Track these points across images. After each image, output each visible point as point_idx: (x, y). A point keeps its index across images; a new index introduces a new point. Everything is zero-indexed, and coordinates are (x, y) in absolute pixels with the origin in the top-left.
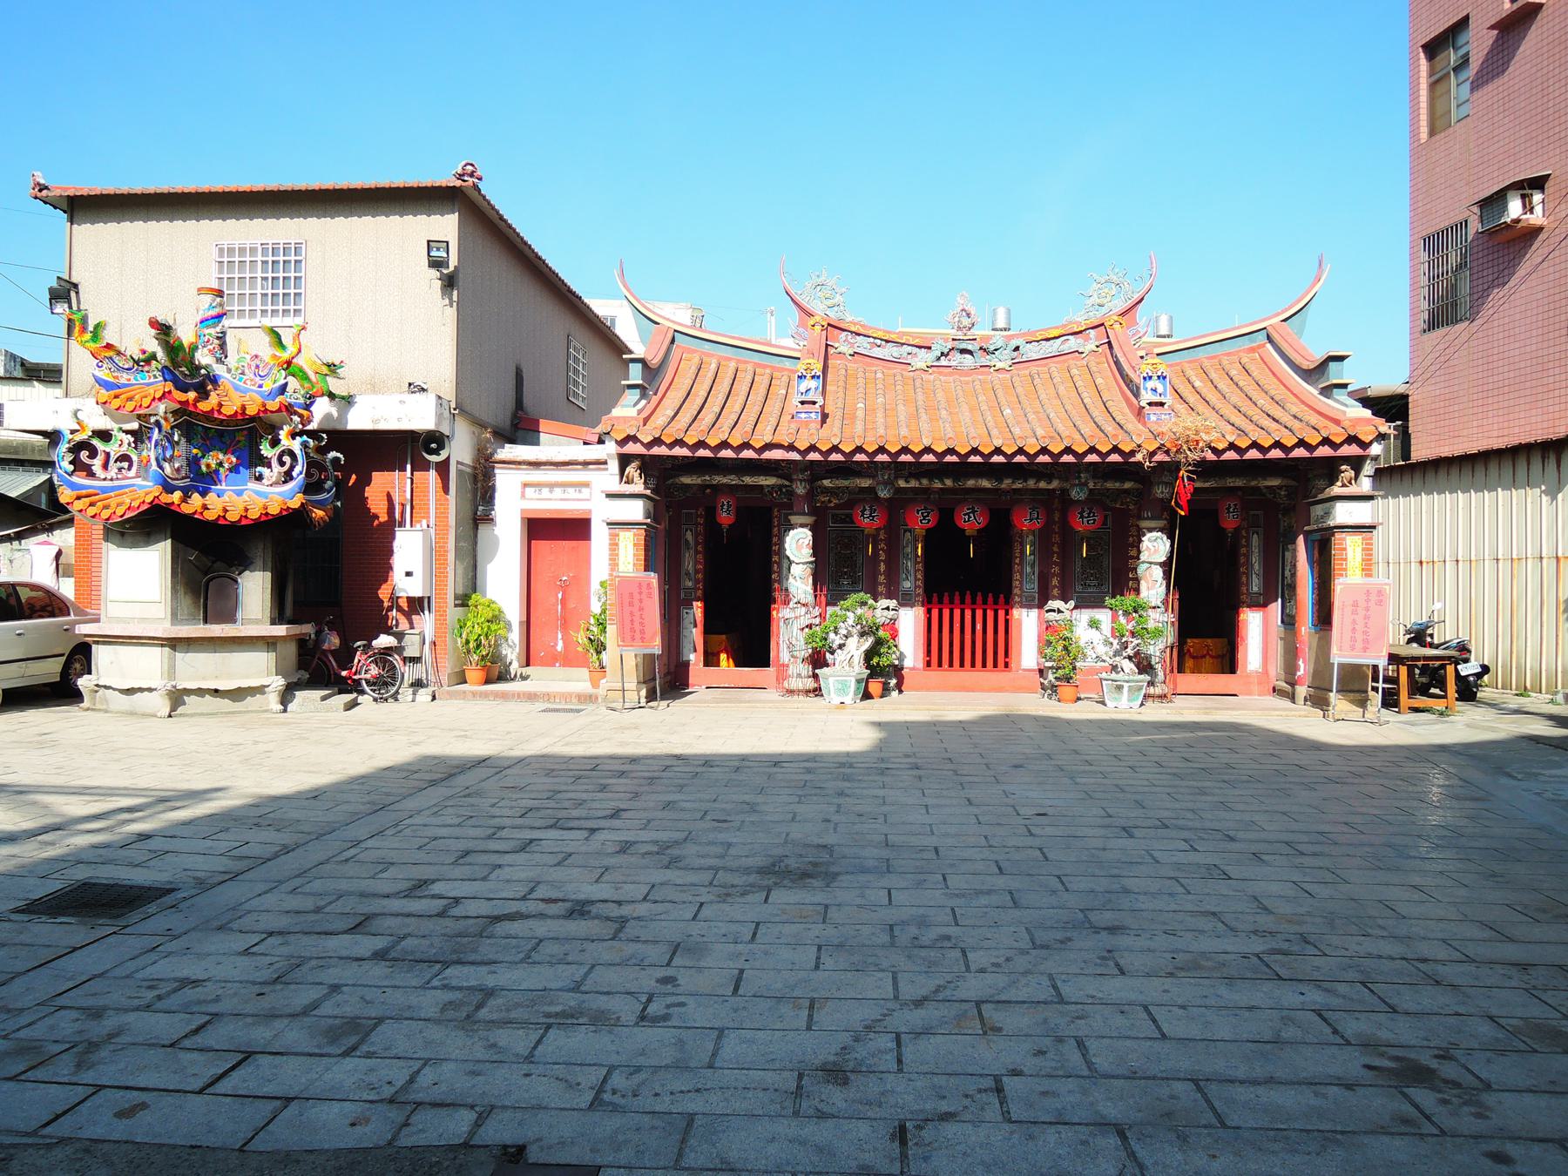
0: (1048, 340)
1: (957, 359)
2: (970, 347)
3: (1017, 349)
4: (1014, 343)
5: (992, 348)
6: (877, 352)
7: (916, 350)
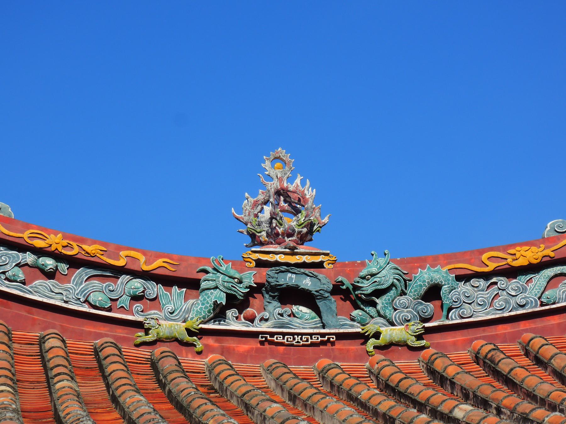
0: (512, 272)
1: (269, 317)
2: (307, 283)
3: (433, 293)
4: (425, 276)
5: (367, 287)
6: (41, 291)
7: (154, 289)
